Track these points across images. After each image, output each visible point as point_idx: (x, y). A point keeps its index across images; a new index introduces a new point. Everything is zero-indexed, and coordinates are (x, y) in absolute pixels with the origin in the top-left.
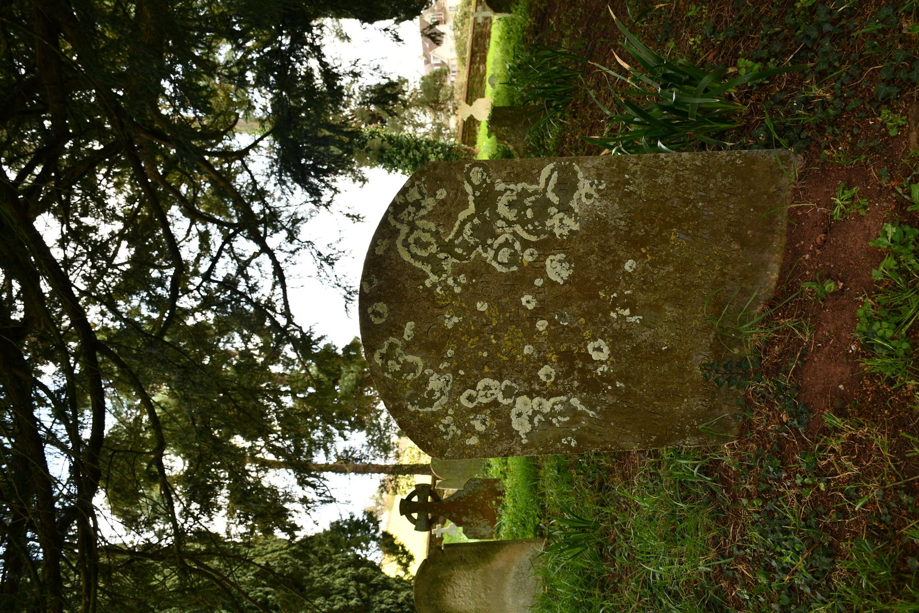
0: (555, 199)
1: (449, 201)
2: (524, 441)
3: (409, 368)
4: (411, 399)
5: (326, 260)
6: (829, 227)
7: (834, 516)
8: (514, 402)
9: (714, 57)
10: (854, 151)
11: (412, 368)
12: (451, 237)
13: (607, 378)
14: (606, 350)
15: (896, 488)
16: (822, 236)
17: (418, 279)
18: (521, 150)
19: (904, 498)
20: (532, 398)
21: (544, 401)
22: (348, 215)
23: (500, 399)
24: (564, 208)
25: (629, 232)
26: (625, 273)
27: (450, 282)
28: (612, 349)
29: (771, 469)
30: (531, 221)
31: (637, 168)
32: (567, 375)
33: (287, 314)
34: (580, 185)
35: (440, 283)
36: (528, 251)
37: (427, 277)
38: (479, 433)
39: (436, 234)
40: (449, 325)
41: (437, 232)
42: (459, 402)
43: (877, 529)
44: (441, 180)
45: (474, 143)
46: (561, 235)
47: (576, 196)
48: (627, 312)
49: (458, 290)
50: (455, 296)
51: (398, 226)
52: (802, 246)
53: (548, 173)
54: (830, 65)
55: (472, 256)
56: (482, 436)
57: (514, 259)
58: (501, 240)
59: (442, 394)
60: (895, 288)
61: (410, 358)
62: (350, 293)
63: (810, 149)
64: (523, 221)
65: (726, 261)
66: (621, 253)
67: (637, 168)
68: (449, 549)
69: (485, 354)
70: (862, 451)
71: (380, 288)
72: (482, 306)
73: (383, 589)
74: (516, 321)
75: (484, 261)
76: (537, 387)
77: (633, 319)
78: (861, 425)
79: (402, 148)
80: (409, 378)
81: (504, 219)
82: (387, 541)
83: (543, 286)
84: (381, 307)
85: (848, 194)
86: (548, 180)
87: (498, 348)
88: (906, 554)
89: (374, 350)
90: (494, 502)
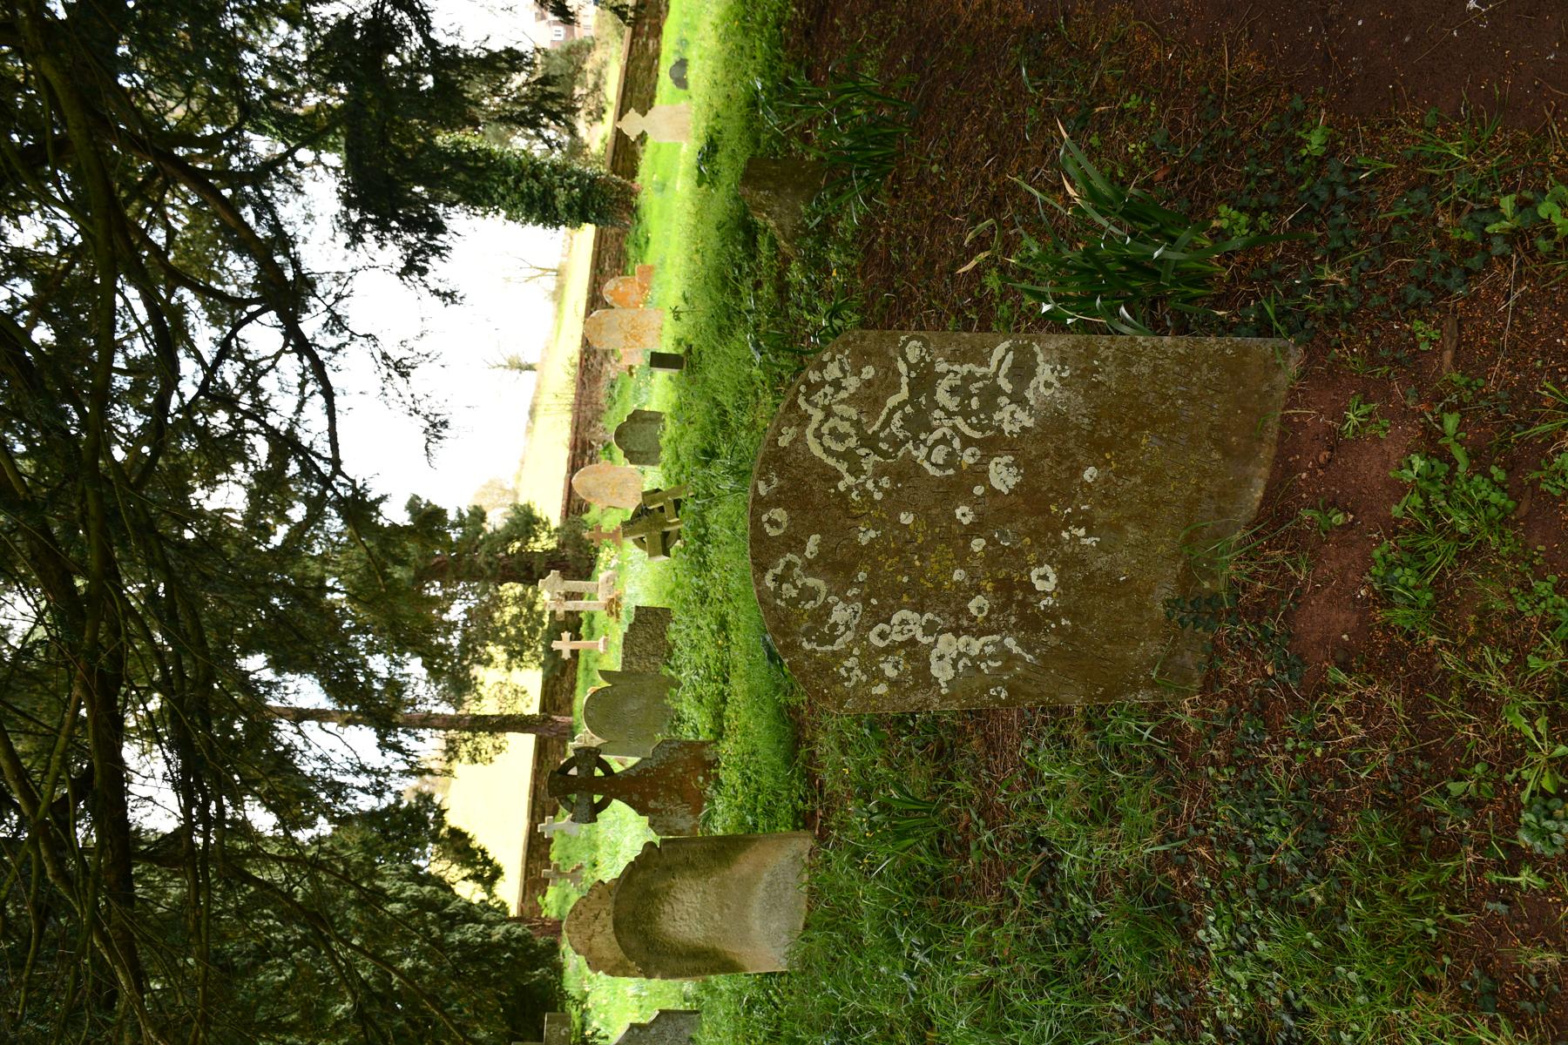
0: (1007, 387)
1: (877, 382)
2: (944, 691)
3: (808, 593)
4: (807, 634)
5: (396, 368)
6: (1335, 442)
7: (1332, 786)
8: (936, 641)
9: (1165, 178)
10: (1373, 360)
11: (812, 594)
12: (875, 428)
13: (1051, 614)
14: (1053, 578)
15: (1408, 754)
16: (1327, 454)
17: (830, 479)
18: (788, 229)
19: (1419, 764)
20: (958, 636)
21: (973, 640)
22: (437, 292)
23: (919, 637)
24: (1018, 399)
25: (1092, 433)
26: (1083, 484)
27: (870, 485)
28: (1059, 578)
29: (1251, 731)
30: (976, 413)
31: (1109, 353)
32: (1003, 608)
33: (336, 462)
34: (1039, 370)
35: (856, 486)
36: (969, 451)
37: (841, 478)
38: (889, 679)
39: (857, 424)
40: (864, 540)
41: (859, 421)
42: (867, 640)
43: (1385, 799)
44: (870, 355)
45: (633, 173)
46: (1011, 432)
47: (1033, 384)
48: (1082, 532)
49: (878, 496)
50: (874, 504)
51: (811, 411)
52: (1297, 461)
53: (1001, 353)
54: (1346, 242)
55: (900, 454)
56: (893, 683)
57: (951, 460)
58: (937, 434)
59: (848, 628)
60: (1420, 529)
61: (811, 582)
62: (434, 426)
63: (1316, 347)
64: (965, 413)
65: (1204, 474)
66: (1081, 459)
67: (1109, 353)
68: (670, 846)
69: (905, 579)
70: (1370, 712)
71: (780, 490)
72: (906, 518)
73: (465, 921)
74: (947, 538)
75: (914, 460)
76: (965, 623)
77: (1088, 541)
78: (1371, 683)
79: (508, 173)
80: (808, 606)
81: (943, 409)
82: (459, 843)
83: (983, 496)
84: (779, 514)
85: (1364, 409)
86: (1001, 362)
87: (922, 572)
88: (1418, 824)
89: (766, 570)
90: (701, 779)
